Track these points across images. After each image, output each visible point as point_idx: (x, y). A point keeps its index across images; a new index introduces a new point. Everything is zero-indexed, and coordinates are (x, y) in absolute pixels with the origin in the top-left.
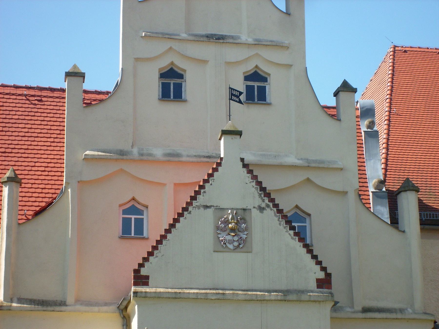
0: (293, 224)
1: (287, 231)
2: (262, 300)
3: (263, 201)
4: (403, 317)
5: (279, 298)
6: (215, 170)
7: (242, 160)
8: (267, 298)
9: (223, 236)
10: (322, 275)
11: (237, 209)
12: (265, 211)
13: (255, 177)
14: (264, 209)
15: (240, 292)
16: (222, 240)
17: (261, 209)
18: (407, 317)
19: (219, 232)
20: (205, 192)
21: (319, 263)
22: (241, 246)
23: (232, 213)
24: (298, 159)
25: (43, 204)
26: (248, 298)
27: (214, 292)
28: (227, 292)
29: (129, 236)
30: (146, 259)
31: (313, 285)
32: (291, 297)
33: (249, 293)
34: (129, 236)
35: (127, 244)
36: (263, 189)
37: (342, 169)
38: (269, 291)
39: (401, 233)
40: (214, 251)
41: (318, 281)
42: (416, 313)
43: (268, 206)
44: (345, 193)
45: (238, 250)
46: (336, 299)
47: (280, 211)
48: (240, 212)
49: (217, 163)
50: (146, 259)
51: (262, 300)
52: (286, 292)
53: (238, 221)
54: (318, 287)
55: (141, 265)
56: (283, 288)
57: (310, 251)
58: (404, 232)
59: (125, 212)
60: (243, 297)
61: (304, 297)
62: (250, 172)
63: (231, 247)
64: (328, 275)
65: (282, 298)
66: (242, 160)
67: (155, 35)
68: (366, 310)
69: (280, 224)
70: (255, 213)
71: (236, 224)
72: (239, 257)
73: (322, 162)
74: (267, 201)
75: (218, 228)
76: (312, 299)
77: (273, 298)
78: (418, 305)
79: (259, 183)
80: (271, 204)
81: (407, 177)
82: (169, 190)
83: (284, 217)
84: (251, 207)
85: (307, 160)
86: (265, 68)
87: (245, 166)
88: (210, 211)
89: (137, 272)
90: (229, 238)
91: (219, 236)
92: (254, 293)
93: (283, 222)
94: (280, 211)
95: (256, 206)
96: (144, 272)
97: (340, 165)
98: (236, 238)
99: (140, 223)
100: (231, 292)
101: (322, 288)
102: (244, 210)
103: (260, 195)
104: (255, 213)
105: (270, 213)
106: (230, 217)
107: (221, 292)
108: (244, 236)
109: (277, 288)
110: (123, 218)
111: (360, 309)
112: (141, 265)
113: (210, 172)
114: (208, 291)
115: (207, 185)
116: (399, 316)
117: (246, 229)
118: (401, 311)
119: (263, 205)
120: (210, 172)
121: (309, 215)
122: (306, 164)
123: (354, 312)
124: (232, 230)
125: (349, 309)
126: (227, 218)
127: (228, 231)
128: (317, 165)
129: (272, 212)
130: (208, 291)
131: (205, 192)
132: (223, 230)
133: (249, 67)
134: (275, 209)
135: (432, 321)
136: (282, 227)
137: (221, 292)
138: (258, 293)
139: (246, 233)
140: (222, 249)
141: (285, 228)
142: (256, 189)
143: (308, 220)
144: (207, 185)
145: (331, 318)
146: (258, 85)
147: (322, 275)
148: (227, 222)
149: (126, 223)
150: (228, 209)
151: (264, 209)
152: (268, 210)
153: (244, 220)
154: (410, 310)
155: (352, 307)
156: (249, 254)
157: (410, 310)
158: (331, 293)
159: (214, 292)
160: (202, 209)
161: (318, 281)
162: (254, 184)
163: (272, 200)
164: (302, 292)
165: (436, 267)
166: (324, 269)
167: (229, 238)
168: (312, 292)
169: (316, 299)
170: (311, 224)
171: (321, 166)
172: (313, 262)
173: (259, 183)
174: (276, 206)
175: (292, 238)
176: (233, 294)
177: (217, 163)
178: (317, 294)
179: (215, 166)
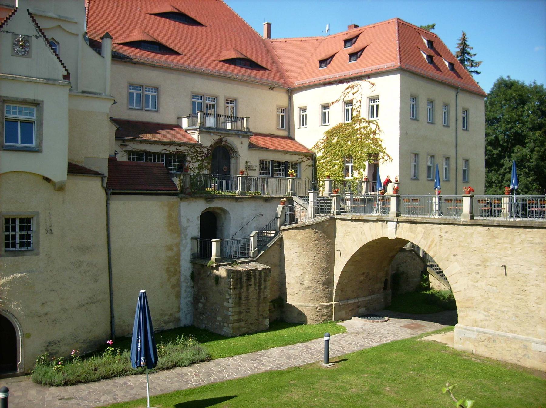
0: (53, 47)
1: (49, 50)
2: (36, 82)
3: (38, 33)
4: (101, 97)
5: (44, 82)
6: (13, 13)
7: (28, 10)
8: (38, 82)
9: (16, 49)
10: (66, 73)
11: (24, 36)
12: (39, 39)
13: (34, 20)
14: (38, 37)
15: (25, 77)
16: (16, 50)
17: (37, 37)
18: (102, 97)
19: (14, 46)
20: (7, 24)
21: (64, 67)
22: (26, 54)
23: (21, 37)
24: (55, 15)
26: (29, 81)
27: (11, 76)
28: (18, 76)
29: (20, 354)
31: (61, 77)
32: (50, 82)
33: (29, 78)
34: (20, 354)
36: (38, 27)
37: (76, 23)
38: (39, 78)
39: (102, 58)
40: (12, 55)
41: (64, 76)
42: (106, 96)
43: (40, 36)
44: (77, 35)
45: (24, 56)
46: (72, 86)
47: (46, 39)
48: (26, 37)
49: (14, 10)
51: (36, 82)
52: (48, 80)
53: (24, 41)
54: (64, 79)
56: (46, 77)
57: (60, 61)
58: (104, 57)
60: (26, 80)
61: (56, 83)
62: (32, 17)
63: (20, 54)
64: (69, 74)
65: (46, 82)
66: (28, 10)
68: (83, 92)
69: (46, 46)
70: (34, 38)
71: (23, 43)
72: (25, 60)
73: (67, 18)
74: (40, 33)
75: (14, 44)
76: (60, 84)
77: (41, 82)
78: (108, 92)
79: (37, 24)
80: (42, 35)
83: (49, 43)
84: (32, 36)
85: (60, 16)
87: (30, 14)
88: (10, 34)
90: (20, 49)
91: (14, 48)
92: (32, 78)
93: (48, 45)
94: (46, 39)
95: (35, 35)
97: (76, 20)
98: (23, 50)
100: (20, 77)
101: (65, 79)
102: (28, 36)
103: (37, 30)
104: (34, 38)
105: (41, 40)
106: (21, 39)
107: (14, 76)
108: (28, 50)
109: (43, 77)
110: (5, 242)
111: (81, 91)
113: (10, 14)
114: (8, 75)
115: (8, 21)
116: (99, 96)
117: (29, 46)
118: (100, 94)
119: (38, 35)
120: (10, 14)
121: (58, 43)
122: (59, 18)
123: (78, 93)
124: (21, 46)
125: (75, 91)
126: (19, 39)
127: (19, 46)
128: (64, 19)
129: (43, 39)
130: (8, 75)
131: (7, 24)
132: (16, 45)
134: (44, 38)
135: (113, 100)
136: (47, 48)
137: (14, 76)
138: (34, 79)
139: (28, 48)
140: (15, 55)
141: (49, 48)
142: (35, 26)
143: (58, 46)
144: (8, 21)
145: (69, 95)
147: (66, 73)
148: (18, 41)
150: (19, 35)
151: (38, 37)
152: (40, 38)
153: (28, 41)
154: (104, 94)
155: (77, 90)
156: (30, 59)
157: (104, 94)
158: (70, 82)
159: (11, 76)
160: (5, 33)
161: (64, 76)
162: (34, 24)
163: (43, 33)
164: (56, 80)
166: (67, 70)
167: (20, 49)
168: (60, 81)
169: (62, 84)
170: (59, 48)
171: (67, 20)
172: (62, 66)
173: (37, 24)
174: (45, 36)
175: (52, 53)
176: (21, 78)
177: (14, 10)
178: (63, 82)
179: (13, 11)
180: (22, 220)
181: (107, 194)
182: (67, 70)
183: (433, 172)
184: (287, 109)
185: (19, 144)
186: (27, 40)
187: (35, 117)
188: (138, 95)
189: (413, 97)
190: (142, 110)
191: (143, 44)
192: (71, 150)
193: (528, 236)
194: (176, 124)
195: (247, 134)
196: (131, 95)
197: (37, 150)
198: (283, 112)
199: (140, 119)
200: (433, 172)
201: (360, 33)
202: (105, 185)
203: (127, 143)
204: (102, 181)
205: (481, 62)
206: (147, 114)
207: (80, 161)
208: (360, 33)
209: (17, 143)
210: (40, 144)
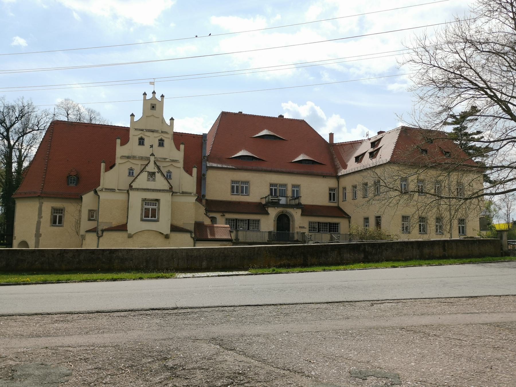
10: (170, 187)
17: (158, 172)
25: (112, 165)
30: (132, 182)
35: (129, 177)
44: (180, 168)
50: (132, 182)
55: (131, 183)
59: (129, 170)
64: (172, 187)
67: (383, 302)
70: (157, 173)
81: (299, 105)
82: (140, 165)
86: (163, 138)
89: (130, 185)
96: (131, 185)
99: (133, 173)
104: (157, 173)
112: (131, 183)
133: (160, 138)
146: (240, 192)
147: (170, 187)
149: (130, 173)
165: (137, 348)
180: (330, 191)
181: (194, 240)
182: (171, 185)
183: (373, 241)
184: (337, 189)
185: (150, 218)
186: (154, 173)
187: (157, 206)
188: (237, 187)
189: (20, 376)
190: (239, 195)
191: (303, 161)
192: (172, 220)
193: (426, 310)
194: (260, 202)
195: (299, 206)
196: (233, 187)
197: (157, 221)
198: (335, 191)
199: (237, 200)
200: (373, 241)
201: (382, 138)
202: (193, 236)
203: (225, 214)
204: (191, 234)
205: (179, 150)
206: (242, 197)
207: (179, 223)
208: (382, 138)
209: (149, 218)
210: (158, 218)
